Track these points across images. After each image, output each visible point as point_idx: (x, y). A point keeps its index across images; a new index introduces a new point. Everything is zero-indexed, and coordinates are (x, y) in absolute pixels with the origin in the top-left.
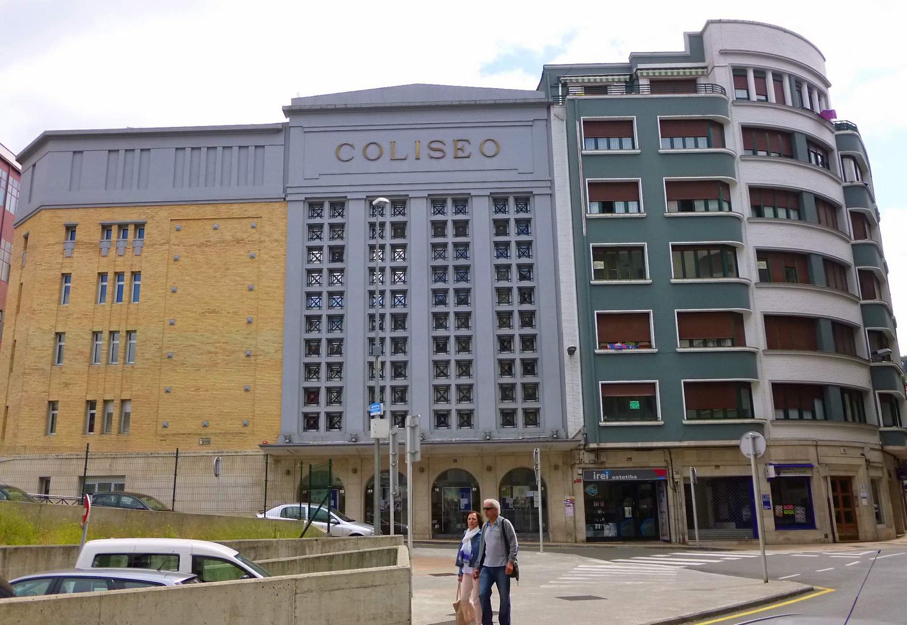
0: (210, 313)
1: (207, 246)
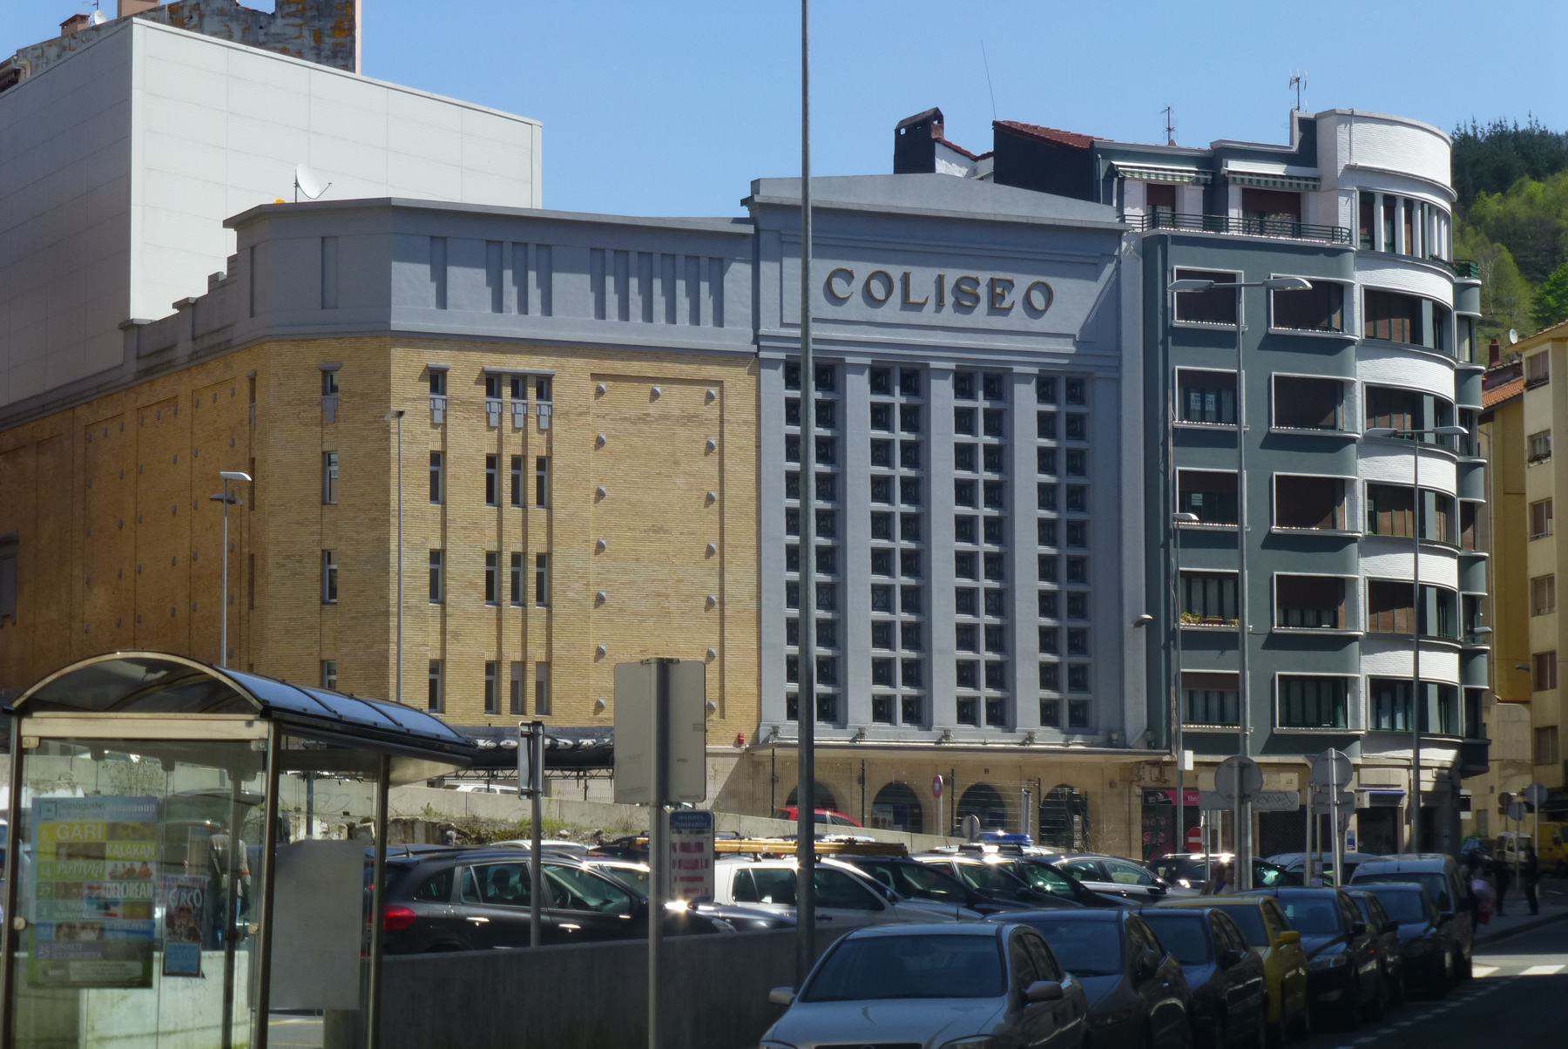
1: (646, 422)
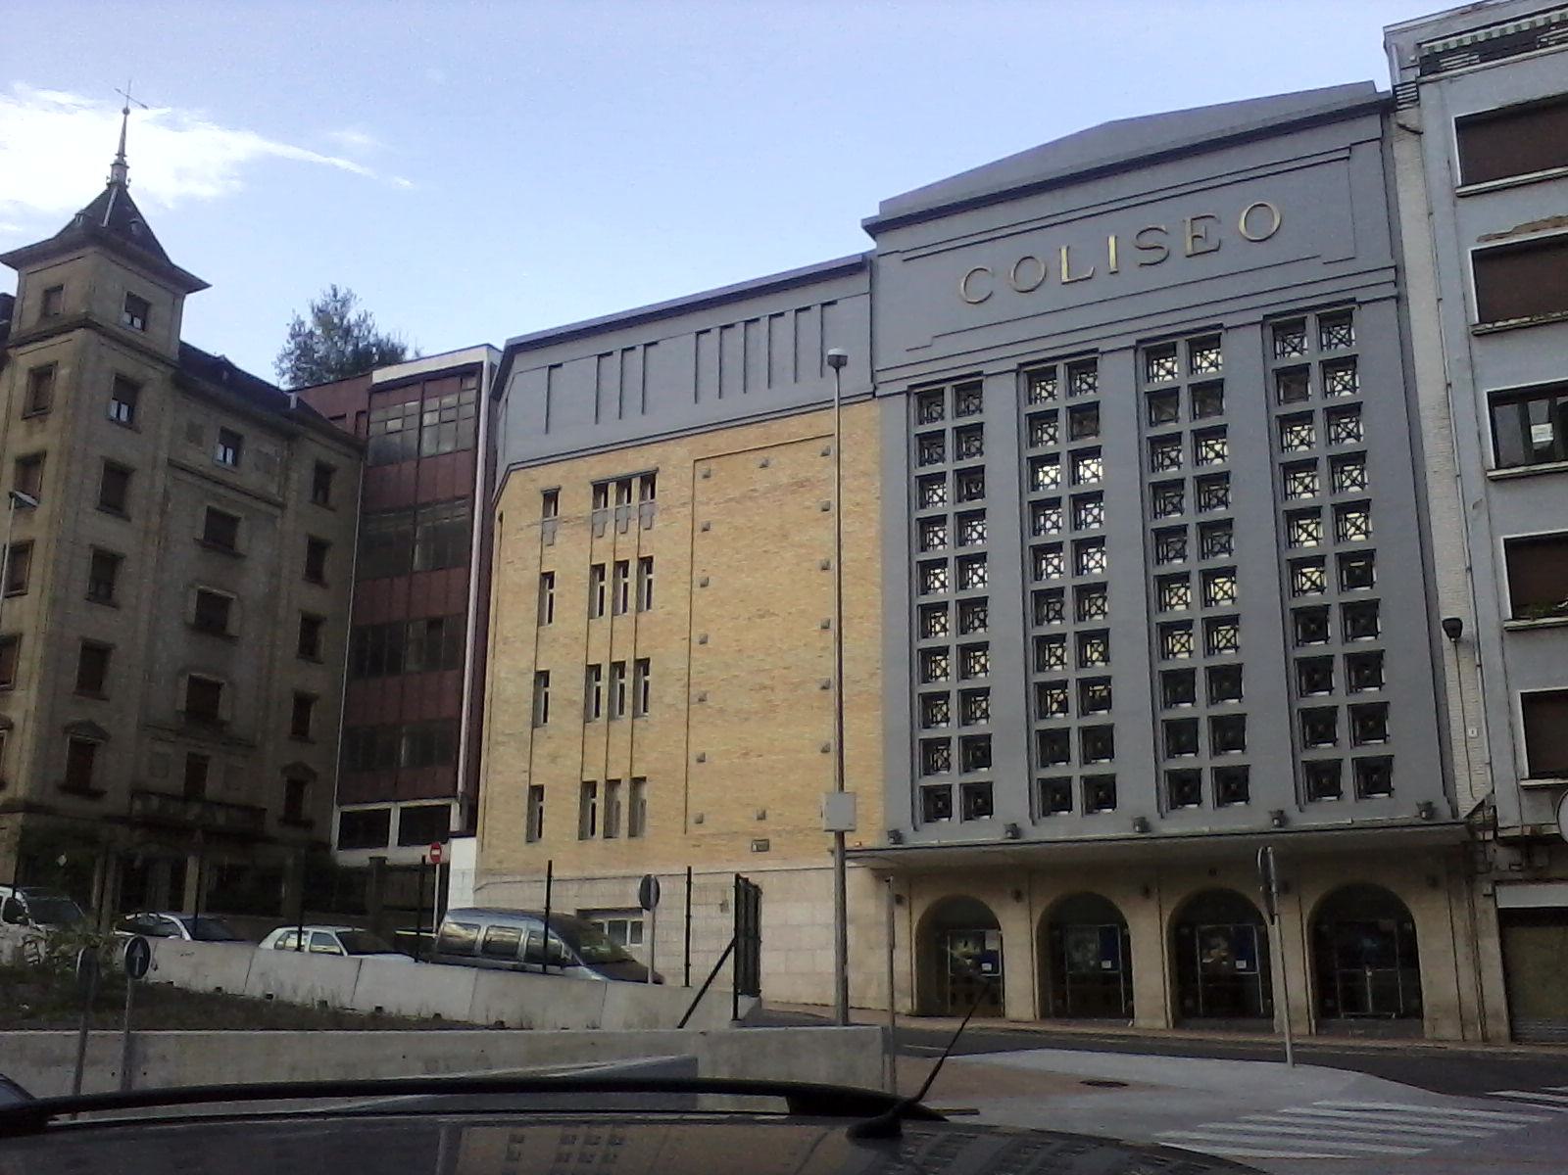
0: (762, 617)
